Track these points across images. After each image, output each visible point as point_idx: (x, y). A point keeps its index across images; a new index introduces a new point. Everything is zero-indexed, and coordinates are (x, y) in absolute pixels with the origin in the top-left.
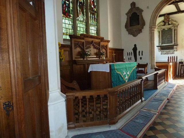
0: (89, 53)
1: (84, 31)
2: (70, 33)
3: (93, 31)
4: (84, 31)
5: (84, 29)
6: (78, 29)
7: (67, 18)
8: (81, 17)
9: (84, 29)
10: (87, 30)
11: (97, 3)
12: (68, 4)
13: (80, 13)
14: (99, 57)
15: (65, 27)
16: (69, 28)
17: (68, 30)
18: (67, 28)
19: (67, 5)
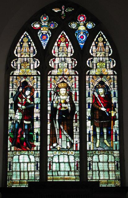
0: (101, 91)
1: (73, 169)
2: (30, 178)
3: (46, 44)
4: (73, 169)
5: (72, 165)
6: (55, 167)
7: (23, 152)
8: (31, 140)
9: (72, 165)
10: (83, 165)
11: (103, 132)
12: (28, 124)
13: (60, 135)
14: (89, 119)
15: (18, 169)
16: (29, 169)
17: (26, 173)
18: (22, 170)
19: (26, 127)
